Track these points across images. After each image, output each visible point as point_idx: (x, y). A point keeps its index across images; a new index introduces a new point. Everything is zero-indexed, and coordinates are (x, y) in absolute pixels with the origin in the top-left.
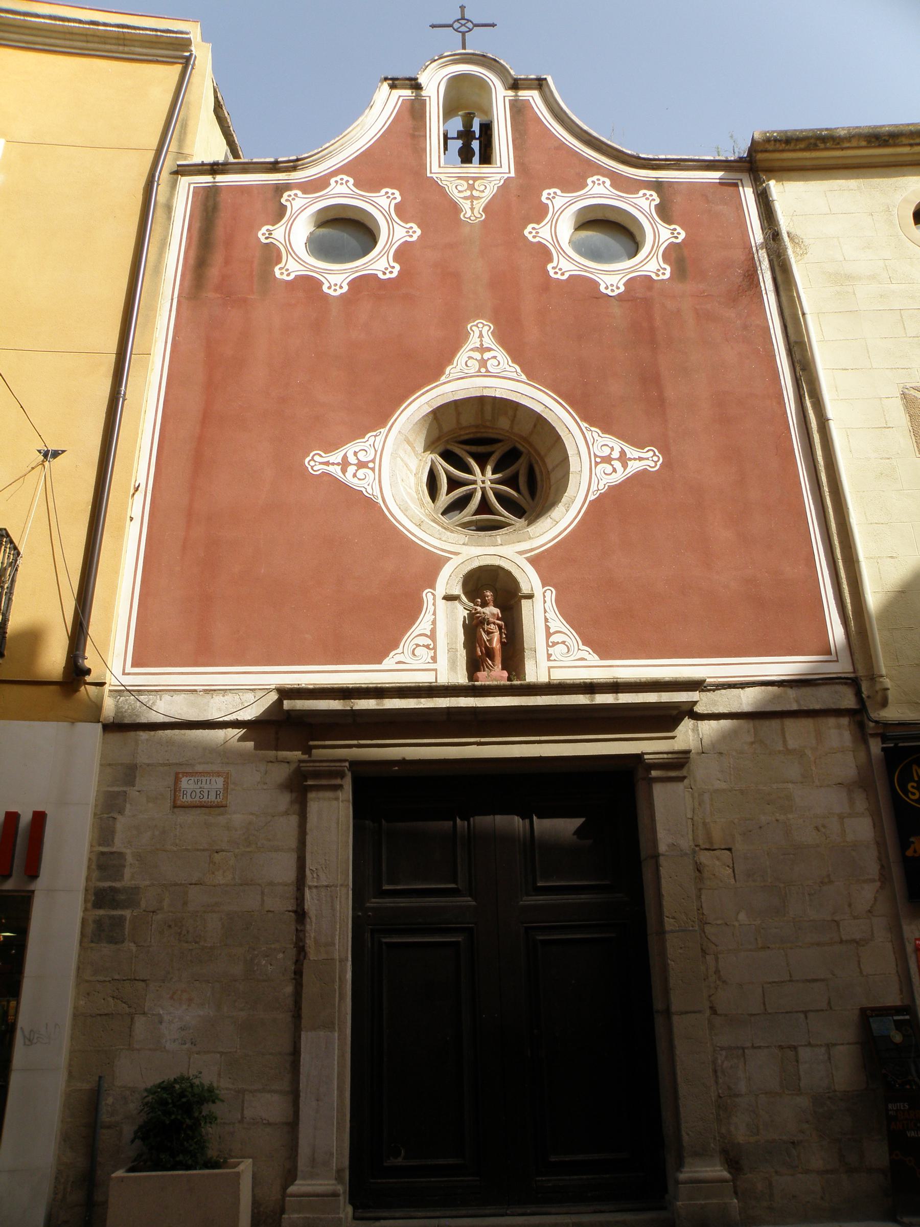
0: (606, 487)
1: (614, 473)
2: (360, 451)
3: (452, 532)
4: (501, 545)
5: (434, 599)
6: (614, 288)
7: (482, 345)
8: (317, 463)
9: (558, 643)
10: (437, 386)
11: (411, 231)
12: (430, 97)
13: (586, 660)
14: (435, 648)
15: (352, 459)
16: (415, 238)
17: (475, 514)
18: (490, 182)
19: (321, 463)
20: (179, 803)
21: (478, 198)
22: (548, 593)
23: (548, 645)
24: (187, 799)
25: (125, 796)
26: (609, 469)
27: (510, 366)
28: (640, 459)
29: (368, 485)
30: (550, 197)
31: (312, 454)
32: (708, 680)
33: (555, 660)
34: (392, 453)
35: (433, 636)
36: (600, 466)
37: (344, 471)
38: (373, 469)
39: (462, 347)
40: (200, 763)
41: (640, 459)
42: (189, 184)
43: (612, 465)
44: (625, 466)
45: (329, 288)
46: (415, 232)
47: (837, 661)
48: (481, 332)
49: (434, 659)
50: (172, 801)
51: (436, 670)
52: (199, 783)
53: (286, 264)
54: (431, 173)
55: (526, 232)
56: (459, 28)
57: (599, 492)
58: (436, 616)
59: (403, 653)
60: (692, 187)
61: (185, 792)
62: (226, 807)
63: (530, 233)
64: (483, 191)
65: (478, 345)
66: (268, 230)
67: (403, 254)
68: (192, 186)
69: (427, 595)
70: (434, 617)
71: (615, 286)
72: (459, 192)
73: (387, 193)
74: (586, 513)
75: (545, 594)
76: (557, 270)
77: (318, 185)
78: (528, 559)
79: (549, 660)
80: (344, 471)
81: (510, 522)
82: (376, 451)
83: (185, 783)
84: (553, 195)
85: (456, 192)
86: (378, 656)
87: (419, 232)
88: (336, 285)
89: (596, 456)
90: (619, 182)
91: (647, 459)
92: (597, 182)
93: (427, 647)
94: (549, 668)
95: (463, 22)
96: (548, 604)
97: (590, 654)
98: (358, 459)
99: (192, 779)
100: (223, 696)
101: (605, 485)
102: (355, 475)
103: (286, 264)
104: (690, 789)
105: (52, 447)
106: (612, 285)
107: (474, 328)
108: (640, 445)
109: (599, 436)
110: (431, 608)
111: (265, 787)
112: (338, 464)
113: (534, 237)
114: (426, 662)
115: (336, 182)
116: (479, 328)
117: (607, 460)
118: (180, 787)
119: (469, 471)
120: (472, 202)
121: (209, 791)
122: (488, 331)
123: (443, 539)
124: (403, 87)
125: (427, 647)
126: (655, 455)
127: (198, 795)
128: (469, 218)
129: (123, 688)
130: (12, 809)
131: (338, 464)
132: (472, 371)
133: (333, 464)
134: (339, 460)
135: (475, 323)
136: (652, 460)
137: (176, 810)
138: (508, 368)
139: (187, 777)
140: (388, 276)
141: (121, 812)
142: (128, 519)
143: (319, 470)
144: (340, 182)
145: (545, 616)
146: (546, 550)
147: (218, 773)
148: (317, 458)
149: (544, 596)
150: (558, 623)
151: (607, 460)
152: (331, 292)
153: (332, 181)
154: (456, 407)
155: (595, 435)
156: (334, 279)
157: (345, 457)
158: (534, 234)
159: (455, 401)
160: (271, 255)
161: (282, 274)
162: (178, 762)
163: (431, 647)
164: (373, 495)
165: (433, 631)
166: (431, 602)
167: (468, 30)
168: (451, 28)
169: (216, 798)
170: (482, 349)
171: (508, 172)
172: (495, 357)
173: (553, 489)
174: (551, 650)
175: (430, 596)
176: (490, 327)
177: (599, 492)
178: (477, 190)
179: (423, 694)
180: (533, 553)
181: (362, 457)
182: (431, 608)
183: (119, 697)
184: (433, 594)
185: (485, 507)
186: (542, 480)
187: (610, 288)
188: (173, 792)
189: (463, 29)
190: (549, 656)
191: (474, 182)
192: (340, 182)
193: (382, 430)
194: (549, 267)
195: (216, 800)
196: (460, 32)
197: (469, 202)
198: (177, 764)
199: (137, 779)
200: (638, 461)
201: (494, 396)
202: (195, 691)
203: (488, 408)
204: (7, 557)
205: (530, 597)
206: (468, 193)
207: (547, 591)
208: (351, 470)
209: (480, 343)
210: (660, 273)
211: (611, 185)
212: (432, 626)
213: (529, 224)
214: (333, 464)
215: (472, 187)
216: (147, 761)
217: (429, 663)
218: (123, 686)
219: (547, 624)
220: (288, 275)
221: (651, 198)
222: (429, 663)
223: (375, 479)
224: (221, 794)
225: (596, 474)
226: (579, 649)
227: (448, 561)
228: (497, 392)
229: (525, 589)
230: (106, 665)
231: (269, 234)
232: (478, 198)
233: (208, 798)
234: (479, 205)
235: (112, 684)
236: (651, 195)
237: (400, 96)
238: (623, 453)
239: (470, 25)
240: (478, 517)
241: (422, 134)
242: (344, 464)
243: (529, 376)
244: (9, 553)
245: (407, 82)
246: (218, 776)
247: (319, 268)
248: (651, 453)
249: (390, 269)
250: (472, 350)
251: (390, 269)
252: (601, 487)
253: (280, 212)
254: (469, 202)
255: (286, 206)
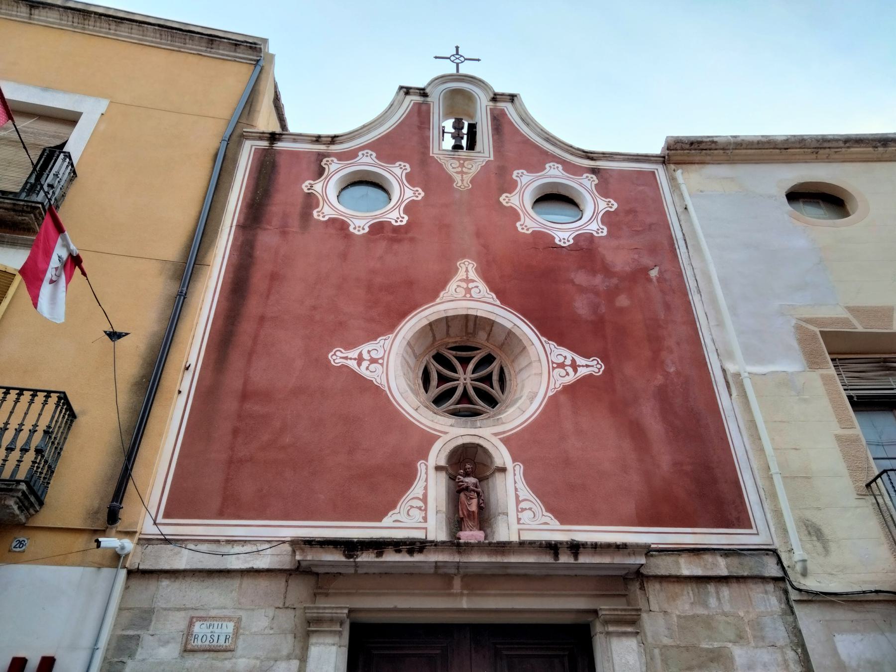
0: (561, 386)
1: (567, 376)
2: (373, 350)
3: (441, 416)
4: (480, 427)
5: (427, 469)
6: (566, 241)
7: (467, 277)
8: (338, 358)
9: (526, 509)
10: (433, 306)
11: (417, 193)
12: (433, 102)
13: (549, 524)
14: (426, 510)
15: (366, 356)
16: (420, 198)
17: (458, 403)
18: (476, 162)
19: (341, 358)
20: (189, 647)
21: (466, 173)
22: (517, 468)
23: (518, 511)
24: (198, 643)
25: (138, 640)
26: (563, 372)
27: (488, 294)
28: (587, 366)
29: (378, 376)
30: (519, 175)
31: (334, 351)
32: (653, 546)
33: (524, 524)
34: (397, 353)
35: (425, 499)
36: (556, 370)
37: (359, 364)
38: (382, 364)
39: (453, 278)
40: (214, 608)
41: (587, 366)
42: (252, 146)
43: (566, 370)
44: (575, 371)
45: (355, 228)
46: (419, 194)
47: (758, 534)
48: (467, 268)
49: (425, 519)
50: (183, 645)
51: (426, 529)
52: (211, 627)
53: (322, 209)
54: (433, 154)
55: (501, 199)
56: (454, 60)
57: (556, 390)
58: (427, 483)
59: (399, 513)
60: (622, 173)
61: (196, 636)
62: (233, 651)
63: (504, 200)
64: (470, 169)
65: (464, 277)
66: (310, 184)
67: (410, 209)
68: (254, 148)
69: (421, 466)
70: (425, 483)
71: (566, 239)
72: (453, 168)
73: (400, 165)
74: (546, 406)
75: (515, 468)
76: (523, 227)
77: (350, 155)
78: (501, 440)
79: (519, 523)
80: (359, 364)
81: (485, 410)
82: (385, 351)
83: (198, 628)
84: (521, 174)
85: (450, 168)
86: (378, 515)
87: (423, 194)
88: (359, 227)
89: (553, 363)
90: (569, 167)
91: (593, 366)
92: (553, 167)
93: (420, 508)
94: (519, 530)
95: (457, 56)
96: (518, 477)
97: (552, 519)
98: (370, 356)
99: (205, 623)
100: (243, 546)
101: (560, 384)
102: (367, 368)
103: (322, 209)
104: (642, 644)
105: (118, 330)
106: (564, 239)
107: (462, 265)
108: (586, 356)
109: (555, 347)
110: (424, 476)
111: (271, 632)
112: (355, 359)
113: (507, 203)
114: (419, 521)
115: (363, 154)
116: (465, 265)
117: (562, 366)
118: (193, 631)
119: (455, 371)
120: (462, 176)
121: (219, 636)
122: (472, 267)
123: (435, 421)
124: (415, 94)
125: (420, 508)
126: (598, 363)
127: (209, 639)
128: (460, 187)
129: (162, 537)
130: (21, 654)
131: (355, 359)
132: (460, 296)
133: (351, 359)
134: (356, 356)
135: (466, 188)
136: (597, 367)
137: (185, 654)
138: (487, 295)
139: (200, 621)
140: (399, 223)
141: (131, 656)
142: (177, 392)
143: (339, 363)
144: (366, 154)
145: (515, 487)
146: (516, 433)
147: (229, 618)
148: (338, 354)
149: (514, 470)
150: (525, 492)
151: (562, 366)
152: (356, 232)
153: (360, 154)
154: (448, 321)
155: (552, 347)
156: (358, 223)
157: (360, 354)
158: (507, 200)
159: (447, 317)
160: (310, 201)
161: (319, 216)
162: (194, 607)
163: (423, 508)
164: (381, 384)
165: (425, 496)
166: (424, 471)
167: (461, 62)
168: (449, 60)
169: (225, 642)
170: (468, 280)
171: (488, 156)
172: (477, 287)
173: (520, 386)
174: (520, 515)
175: (423, 467)
176: (474, 265)
177: (556, 390)
178: (466, 168)
179: (427, 546)
180: (505, 435)
181: (374, 355)
182: (424, 476)
183: (147, 545)
184: (425, 465)
185: (465, 397)
186: (510, 380)
187: (563, 241)
188: (185, 636)
189: (457, 61)
190: (519, 520)
191: (464, 162)
192: (366, 154)
193: (390, 336)
194: (518, 224)
195: (225, 644)
196: (455, 63)
197: (460, 175)
198: (192, 609)
199: (153, 623)
200: (585, 367)
201: (475, 314)
202: (218, 541)
203: (471, 324)
204: (64, 422)
205: (503, 470)
206: (460, 169)
207: (517, 466)
208: (365, 364)
209: (466, 276)
210: (599, 232)
211: (563, 169)
212: (424, 491)
213: (504, 193)
214: (351, 359)
215: (462, 166)
216: (164, 606)
217: (420, 522)
218: (162, 534)
219: (517, 493)
220: (324, 217)
221: (592, 180)
222: (420, 522)
223: (383, 372)
224: (230, 639)
225: (553, 376)
226: (543, 515)
227: (437, 440)
228: (478, 312)
229: (498, 463)
230: (143, 503)
231: (310, 187)
232: (466, 173)
233: (217, 642)
234: (467, 178)
235: (142, 533)
236: (592, 178)
237: (412, 100)
238: (573, 361)
239: (462, 59)
240: (459, 406)
241: (427, 126)
242: (360, 360)
243: (502, 302)
244: (69, 425)
245: (418, 91)
246: (230, 621)
247: (348, 214)
248: (595, 362)
249: (401, 219)
250: (460, 280)
251: (401, 219)
252: (557, 386)
253: (320, 172)
254: (460, 175)
255: (325, 168)
